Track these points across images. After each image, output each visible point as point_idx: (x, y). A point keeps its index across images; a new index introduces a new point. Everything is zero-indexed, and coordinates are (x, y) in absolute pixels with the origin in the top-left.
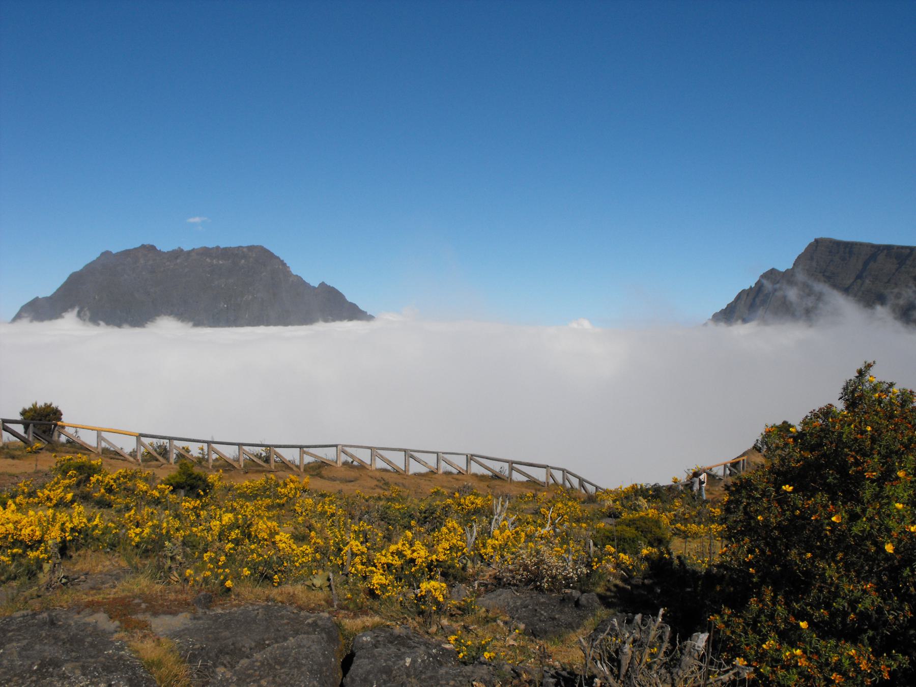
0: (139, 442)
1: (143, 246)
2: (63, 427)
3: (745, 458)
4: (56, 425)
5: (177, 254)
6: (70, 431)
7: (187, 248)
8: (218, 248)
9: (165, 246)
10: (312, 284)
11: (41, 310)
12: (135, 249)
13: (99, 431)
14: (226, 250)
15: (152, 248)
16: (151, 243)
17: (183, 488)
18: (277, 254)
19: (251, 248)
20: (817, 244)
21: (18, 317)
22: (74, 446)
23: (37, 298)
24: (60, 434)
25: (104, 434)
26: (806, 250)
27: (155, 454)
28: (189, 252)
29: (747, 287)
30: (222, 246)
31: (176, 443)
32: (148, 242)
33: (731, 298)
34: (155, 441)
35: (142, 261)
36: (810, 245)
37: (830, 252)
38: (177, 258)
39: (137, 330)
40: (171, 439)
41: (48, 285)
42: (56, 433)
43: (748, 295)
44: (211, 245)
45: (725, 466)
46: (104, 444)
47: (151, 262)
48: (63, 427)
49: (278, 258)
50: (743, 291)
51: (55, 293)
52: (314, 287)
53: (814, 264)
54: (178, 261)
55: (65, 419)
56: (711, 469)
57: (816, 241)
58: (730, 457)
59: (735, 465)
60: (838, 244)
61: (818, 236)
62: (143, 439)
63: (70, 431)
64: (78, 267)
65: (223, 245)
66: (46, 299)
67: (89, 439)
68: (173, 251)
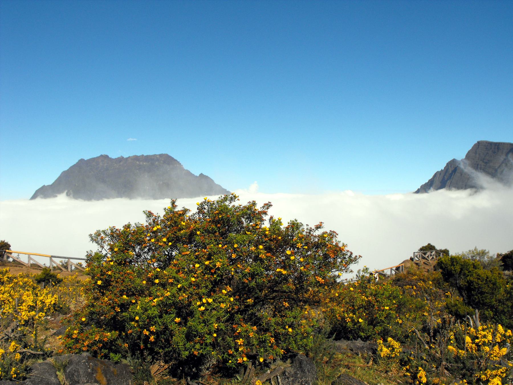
0: (51, 261)
1: (102, 156)
2: (11, 253)
3: (403, 264)
4: (5, 252)
5: (121, 160)
6: (14, 255)
7: (125, 156)
8: (143, 155)
9: (114, 155)
10: (195, 175)
11: (44, 192)
12: (97, 157)
13: (29, 255)
14: (147, 156)
15: (107, 157)
16: (106, 154)
17: (44, 281)
18: (175, 158)
19: (161, 155)
20: (479, 144)
21: (34, 197)
22: (17, 264)
23: (44, 185)
24: (8, 257)
25: (31, 256)
26: (473, 147)
27: (60, 267)
28: (127, 158)
29: (440, 170)
30: (145, 155)
31: (71, 260)
32: (104, 153)
33: (430, 177)
34: (63, 260)
35: (101, 164)
36: (475, 145)
37: (486, 148)
38: (120, 162)
39: (87, 203)
40: (69, 258)
41: (50, 178)
42: (5, 257)
43: (440, 174)
44: (139, 154)
45: (391, 269)
46: (32, 262)
47: (106, 165)
48: (11, 253)
49: (176, 160)
50: (438, 172)
51: (53, 183)
52: (197, 176)
53: (477, 155)
54: (121, 163)
55: (13, 249)
56: (383, 271)
57: (478, 142)
58: (397, 264)
59: (398, 268)
60: (491, 144)
61: (479, 140)
62: (53, 259)
63: (14, 255)
64: (66, 168)
65: (145, 154)
66: (48, 186)
67: (24, 259)
68: (118, 158)
